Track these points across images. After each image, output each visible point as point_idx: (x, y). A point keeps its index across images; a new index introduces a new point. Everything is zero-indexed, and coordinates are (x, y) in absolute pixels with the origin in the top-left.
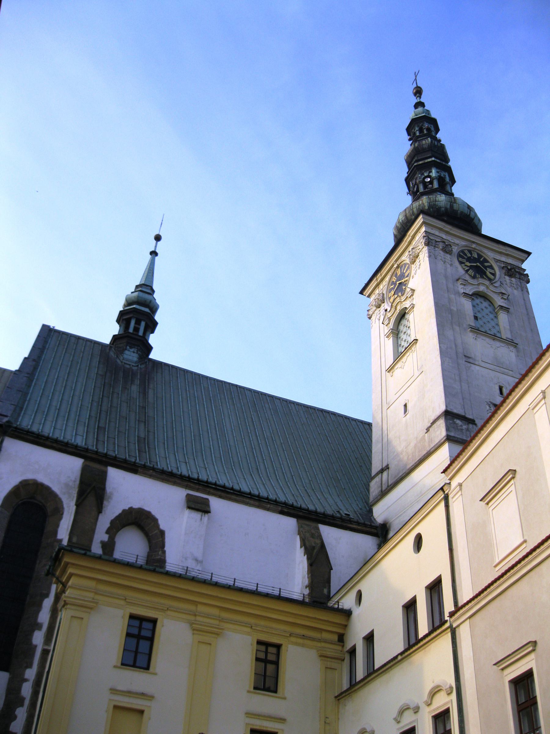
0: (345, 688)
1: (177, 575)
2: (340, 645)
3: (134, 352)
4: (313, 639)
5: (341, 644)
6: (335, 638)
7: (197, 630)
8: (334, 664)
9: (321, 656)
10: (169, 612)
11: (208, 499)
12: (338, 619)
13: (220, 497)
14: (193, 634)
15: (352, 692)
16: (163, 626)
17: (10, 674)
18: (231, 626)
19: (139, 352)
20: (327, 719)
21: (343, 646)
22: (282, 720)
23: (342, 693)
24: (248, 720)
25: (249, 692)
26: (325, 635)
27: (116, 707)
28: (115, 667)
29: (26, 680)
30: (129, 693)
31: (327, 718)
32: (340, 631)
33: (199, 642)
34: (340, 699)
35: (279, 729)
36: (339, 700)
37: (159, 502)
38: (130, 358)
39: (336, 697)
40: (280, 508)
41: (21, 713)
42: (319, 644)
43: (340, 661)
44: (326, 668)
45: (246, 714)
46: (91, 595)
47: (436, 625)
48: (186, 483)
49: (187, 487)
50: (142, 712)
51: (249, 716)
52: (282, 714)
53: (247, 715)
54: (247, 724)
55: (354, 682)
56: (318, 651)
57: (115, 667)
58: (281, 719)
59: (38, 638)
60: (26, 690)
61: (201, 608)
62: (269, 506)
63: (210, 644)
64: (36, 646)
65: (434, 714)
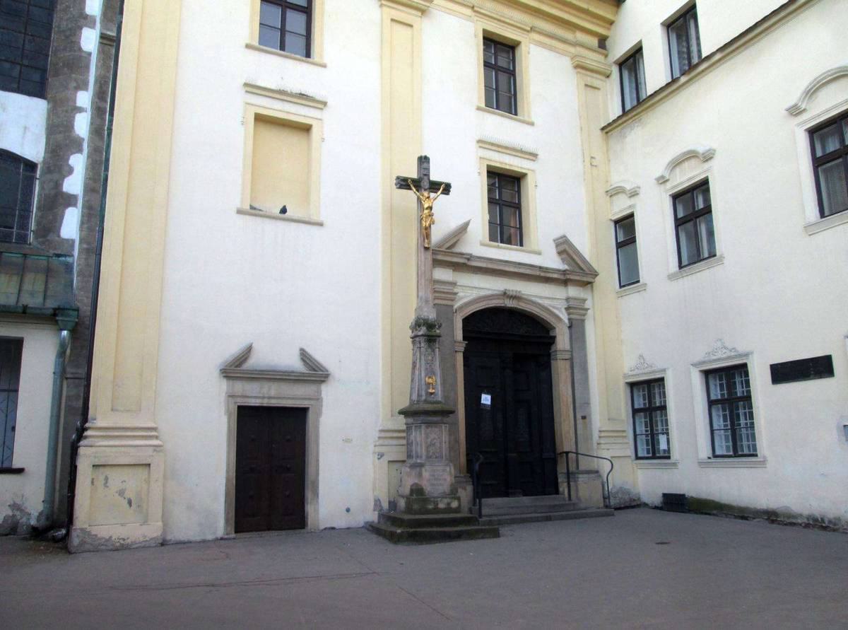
0: (612, 117)
2: (602, 54)
4: (564, 41)
5: (603, 51)
6: (594, 42)
8: (596, 81)
9: (577, 67)
15: (643, 111)
17: (48, 102)
20: (593, 160)
21: (606, 56)
22: (533, 156)
23: (609, 125)
25: (479, 109)
26: (580, 36)
27: (260, 119)
28: (248, 46)
29: (80, 110)
30: (281, 94)
31: (592, 158)
34: (611, 131)
35: (529, 170)
36: (607, 133)
39: (603, 129)
41: (78, 162)
42: (572, 50)
43: (603, 78)
45: (246, 85)
47: (628, 107)
50: (149, 465)
51: (483, 145)
52: (529, 146)
53: (481, 145)
54: (231, 396)
55: (643, 96)
56: (572, 59)
57: (248, 46)
58: (531, 154)
59: (89, 40)
60: (82, 125)
63: (411, 26)
64: (90, 54)
65: (671, 193)
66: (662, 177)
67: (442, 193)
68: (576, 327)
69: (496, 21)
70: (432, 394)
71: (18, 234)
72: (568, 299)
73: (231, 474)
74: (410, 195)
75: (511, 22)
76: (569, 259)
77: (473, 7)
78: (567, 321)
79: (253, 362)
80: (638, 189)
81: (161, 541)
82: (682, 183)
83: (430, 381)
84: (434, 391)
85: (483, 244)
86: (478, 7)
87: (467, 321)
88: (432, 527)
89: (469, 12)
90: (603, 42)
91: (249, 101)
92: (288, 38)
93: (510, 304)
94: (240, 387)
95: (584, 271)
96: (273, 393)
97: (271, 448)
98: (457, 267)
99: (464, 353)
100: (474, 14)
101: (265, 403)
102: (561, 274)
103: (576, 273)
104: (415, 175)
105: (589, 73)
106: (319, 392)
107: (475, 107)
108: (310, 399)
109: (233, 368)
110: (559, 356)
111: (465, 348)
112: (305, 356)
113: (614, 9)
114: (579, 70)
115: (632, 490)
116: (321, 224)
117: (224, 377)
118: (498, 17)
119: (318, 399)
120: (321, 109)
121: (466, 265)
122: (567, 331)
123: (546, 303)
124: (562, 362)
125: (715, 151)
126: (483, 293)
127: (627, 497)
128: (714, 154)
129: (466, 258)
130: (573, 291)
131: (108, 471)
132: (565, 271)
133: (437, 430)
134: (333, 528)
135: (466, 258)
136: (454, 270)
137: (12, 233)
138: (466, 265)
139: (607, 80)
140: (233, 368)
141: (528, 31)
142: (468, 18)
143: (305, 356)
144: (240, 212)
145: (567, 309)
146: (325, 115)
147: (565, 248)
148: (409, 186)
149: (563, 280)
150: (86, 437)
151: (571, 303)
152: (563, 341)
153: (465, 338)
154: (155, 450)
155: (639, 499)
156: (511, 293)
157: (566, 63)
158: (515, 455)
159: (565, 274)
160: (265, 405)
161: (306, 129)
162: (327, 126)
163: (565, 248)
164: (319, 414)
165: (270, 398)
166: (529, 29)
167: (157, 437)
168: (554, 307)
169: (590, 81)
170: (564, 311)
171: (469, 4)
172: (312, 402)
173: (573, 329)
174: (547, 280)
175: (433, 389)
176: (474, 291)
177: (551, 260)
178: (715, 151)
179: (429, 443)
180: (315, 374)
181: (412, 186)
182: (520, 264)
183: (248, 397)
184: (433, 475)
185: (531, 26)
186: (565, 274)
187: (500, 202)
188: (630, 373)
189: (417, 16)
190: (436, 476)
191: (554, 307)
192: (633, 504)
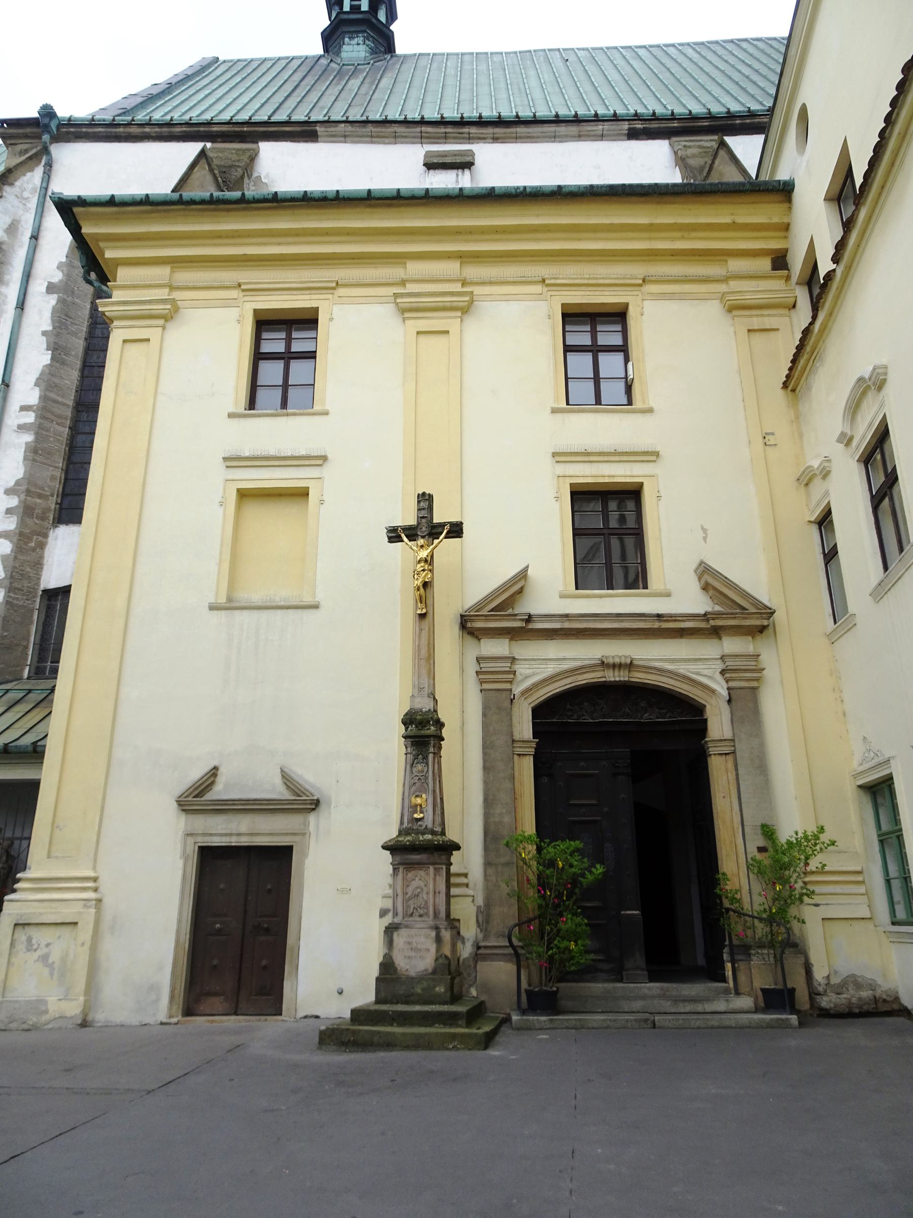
1: (330, 196)
2: (781, 277)
3: (358, 44)
6: (765, 264)
7: (411, 310)
10: (341, 291)
11: (471, 150)
12: (762, 213)
13: (495, 139)
14: (404, 319)
16: (331, 319)
18: (487, 290)
19: (367, 42)
22: (652, 456)
24: (561, 469)
26: (736, 265)
27: (244, 495)
32: (775, 245)
33: (418, 333)
37: (371, 179)
38: (355, 54)
40: (626, 126)
42: (722, 288)
43: (786, 311)
44: (749, 331)
45: (554, 455)
46: (163, 293)
48: (418, 129)
49: (422, 139)
50: (302, 494)
52: (644, 443)
53: (558, 459)
56: (721, 299)
61: (414, 268)
62: (601, 127)
66: (843, 434)
67: (446, 537)
68: (745, 698)
69: (583, 288)
70: (418, 820)
71: (51, 667)
72: (723, 658)
73: (182, 938)
74: (404, 550)
75: (607, 282)
76: (718, 595)
77: (544, 281)
78: (725, 693)
79: (219, 791)
80: (826, 464)
81: (79, 1022)
82: (864, 436)
83: (419, 801)
84: (422, 815)
85: (563, 596)
86: (551, 279)
87: (538, 711)
88: (431, 1025)
89: (538, 288)
90: (780, 261)
91: (231, 477)
92: (261, 394)
93: (612, 676)
94: (202, 823)
95: (744, 609)
96: (243, 829)
97: (241, 903)
98: (513, 634)
99: (535, 757)
100: (545, 289)
101: (234, 841)
102: (703, 620)
103: (736, 616)
104: (412, 521)
105: (754, 312)
106: (306, 824)
107: (549, 410)
108: (294, 834)
109: (190, 799)
110: (712, 750)
111: (536, 749)
112: (287, 778)
113: (786, 205)
114: (735, 313)
115: (879, 981)
116: (316, 607)
117: (183, 810)
118: (586, 282)
119: (304, 834)
120: (654, 461)
121: (527, 630)
122: (725, 709)
123: (682, 669)
124: (719, 758)
125: (886, 367)
126: (566, 666)
127: (865, 994)
128: (886, 374)
129: (522, 620)
130: (732, 645)
131: (33, 932)
132: (705, 615)
133: (422, 873)
134: (317, 1017)
135: (522, 620)
136: (511, 639)
137: (45, 668)
138: (527, 630)
139: (793, 311)
140: (190, 799)
141: (640, 285)
142: (539, 297)
143: (287, 778)
144: (213, 608)
145: (723, 672)
146: (326, 471)
147: (709, 579)
148: (400, 537)
149: (708, 628)
150: (14, 891)
151: (730, 663)
152: (719, 725)
153: (535, 735)
154: (85, 906)
155: (897, 999)
156: (611, 661)
157: (714, 309)
158: (637, 912)
159: (708, 620)
160: (233, 844)
161: (302, 494)
162: (329, 488)
163: (709, 579)
164: (304, 855)
165: (239, 835)
166: (641, 282)
167: (467, 885)
168: (698, 674)
169: (756, 323)
170: (718, 677)
171: (536, 279)
172: (296, 838)
173: (733, 702)
174: (681, 633)
175: (422, 812)
176: (545, 666)
177: (689, 600)
178: (886, 367)
179: (410, 894)
180: (305, 803)
181: (403, 536)
182: (619, 615)
183: (211, 835)
184: (409, 943)
185: (642, 276)
186: (708, 620)
187: (605, 531)
188: (861, 769)
189: (781, 315)
190: (414, 945)
191: (698, 674)
192: (883, 1008)
